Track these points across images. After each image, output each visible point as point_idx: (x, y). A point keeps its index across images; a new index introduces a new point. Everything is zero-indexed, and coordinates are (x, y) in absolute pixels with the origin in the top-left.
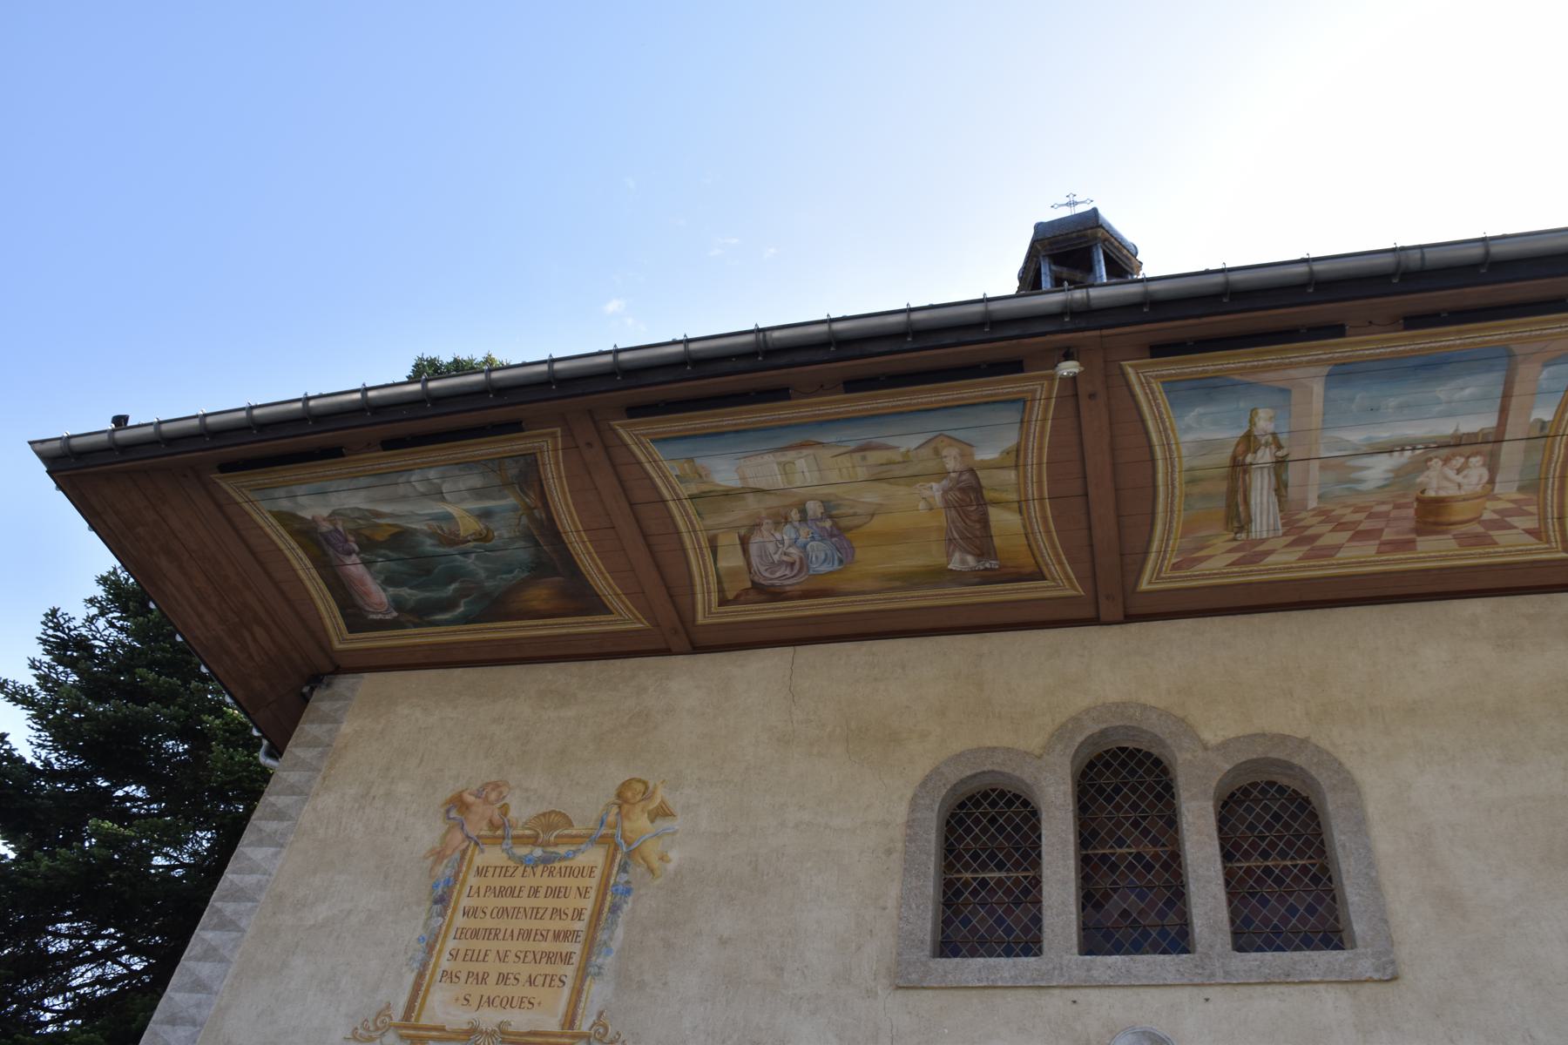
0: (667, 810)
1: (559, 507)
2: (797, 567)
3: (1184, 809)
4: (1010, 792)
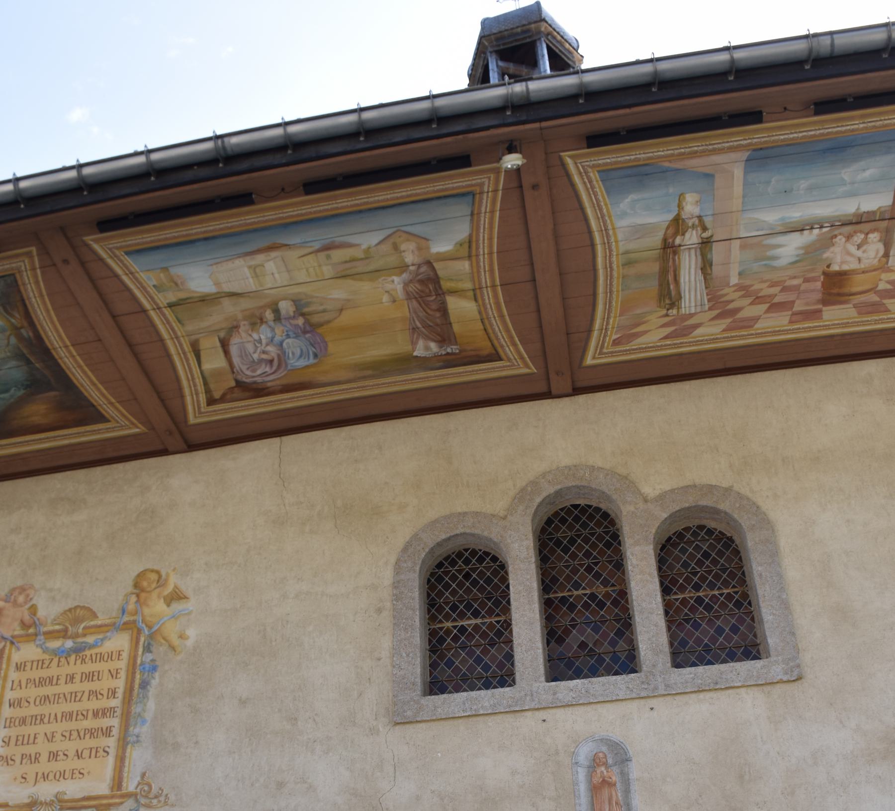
0: (179, 593)
1: (45, 324)
2: (276, 363)
3: (628, 554)
4: (480, 550)
